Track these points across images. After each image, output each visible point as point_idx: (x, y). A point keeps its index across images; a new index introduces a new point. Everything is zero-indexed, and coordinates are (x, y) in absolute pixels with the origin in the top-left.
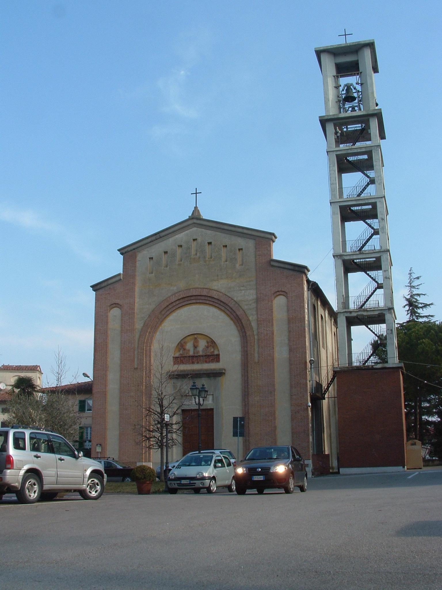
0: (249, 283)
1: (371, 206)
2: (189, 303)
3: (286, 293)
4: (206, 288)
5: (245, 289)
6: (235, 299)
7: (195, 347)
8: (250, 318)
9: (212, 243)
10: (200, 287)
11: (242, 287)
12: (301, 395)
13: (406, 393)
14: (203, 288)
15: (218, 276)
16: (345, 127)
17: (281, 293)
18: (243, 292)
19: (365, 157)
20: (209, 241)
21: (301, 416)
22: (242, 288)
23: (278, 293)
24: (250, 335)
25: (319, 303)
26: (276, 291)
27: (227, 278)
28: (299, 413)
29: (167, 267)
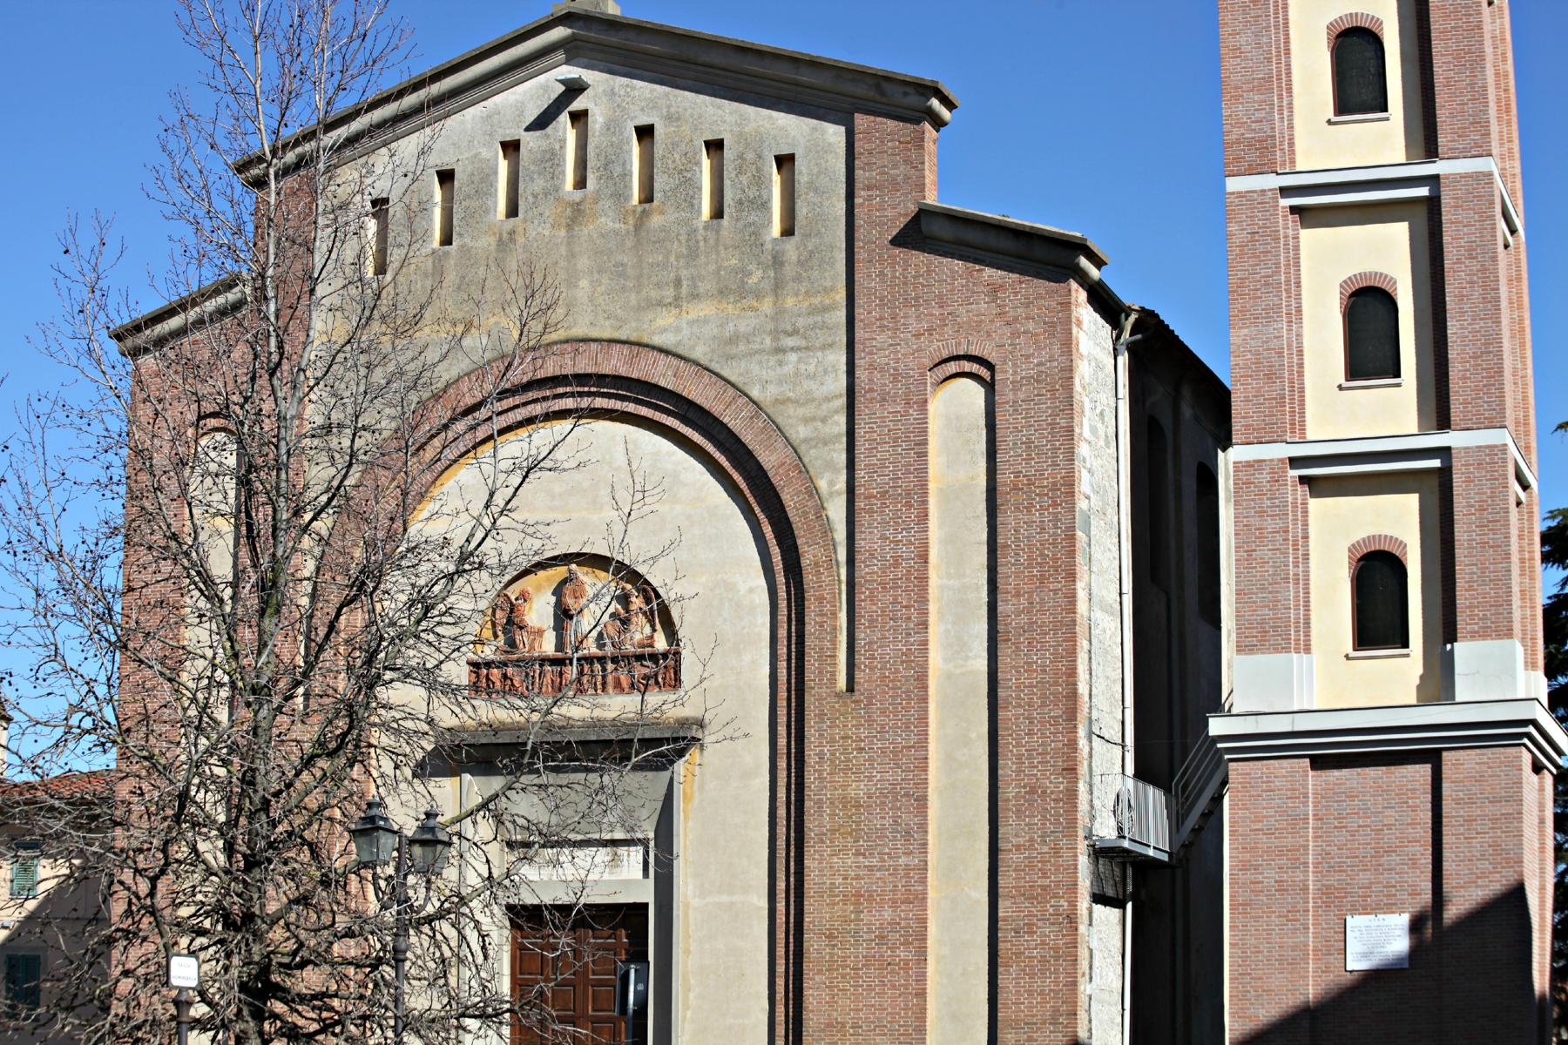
0: (819, 319)
1: (1439, 461)
2: (510, 414)
3: (990, 367)
4: (624, 338)
5: (803, 343)
6: (755, 393)
7: (563, 615)
8: (822, 484)
9: (656, 133)
10: (595, 334)
11: (790, 335)
12: (1046, 849)
13: (1560, 922)
14: (611, 341)
15: (678, 283)
16: (1555, 1031)
17: (967, 366)
18: (793, 357)
19: (1436, 463)
20: (644, 120)
21: (1043, 943)
22: (790, 342)
23: (953, 367)
24: (816, 564)
25: (1187, 412)
26: (945, 354)
27: (721, 292)
28: (1031, 933)
29: (451, 244)
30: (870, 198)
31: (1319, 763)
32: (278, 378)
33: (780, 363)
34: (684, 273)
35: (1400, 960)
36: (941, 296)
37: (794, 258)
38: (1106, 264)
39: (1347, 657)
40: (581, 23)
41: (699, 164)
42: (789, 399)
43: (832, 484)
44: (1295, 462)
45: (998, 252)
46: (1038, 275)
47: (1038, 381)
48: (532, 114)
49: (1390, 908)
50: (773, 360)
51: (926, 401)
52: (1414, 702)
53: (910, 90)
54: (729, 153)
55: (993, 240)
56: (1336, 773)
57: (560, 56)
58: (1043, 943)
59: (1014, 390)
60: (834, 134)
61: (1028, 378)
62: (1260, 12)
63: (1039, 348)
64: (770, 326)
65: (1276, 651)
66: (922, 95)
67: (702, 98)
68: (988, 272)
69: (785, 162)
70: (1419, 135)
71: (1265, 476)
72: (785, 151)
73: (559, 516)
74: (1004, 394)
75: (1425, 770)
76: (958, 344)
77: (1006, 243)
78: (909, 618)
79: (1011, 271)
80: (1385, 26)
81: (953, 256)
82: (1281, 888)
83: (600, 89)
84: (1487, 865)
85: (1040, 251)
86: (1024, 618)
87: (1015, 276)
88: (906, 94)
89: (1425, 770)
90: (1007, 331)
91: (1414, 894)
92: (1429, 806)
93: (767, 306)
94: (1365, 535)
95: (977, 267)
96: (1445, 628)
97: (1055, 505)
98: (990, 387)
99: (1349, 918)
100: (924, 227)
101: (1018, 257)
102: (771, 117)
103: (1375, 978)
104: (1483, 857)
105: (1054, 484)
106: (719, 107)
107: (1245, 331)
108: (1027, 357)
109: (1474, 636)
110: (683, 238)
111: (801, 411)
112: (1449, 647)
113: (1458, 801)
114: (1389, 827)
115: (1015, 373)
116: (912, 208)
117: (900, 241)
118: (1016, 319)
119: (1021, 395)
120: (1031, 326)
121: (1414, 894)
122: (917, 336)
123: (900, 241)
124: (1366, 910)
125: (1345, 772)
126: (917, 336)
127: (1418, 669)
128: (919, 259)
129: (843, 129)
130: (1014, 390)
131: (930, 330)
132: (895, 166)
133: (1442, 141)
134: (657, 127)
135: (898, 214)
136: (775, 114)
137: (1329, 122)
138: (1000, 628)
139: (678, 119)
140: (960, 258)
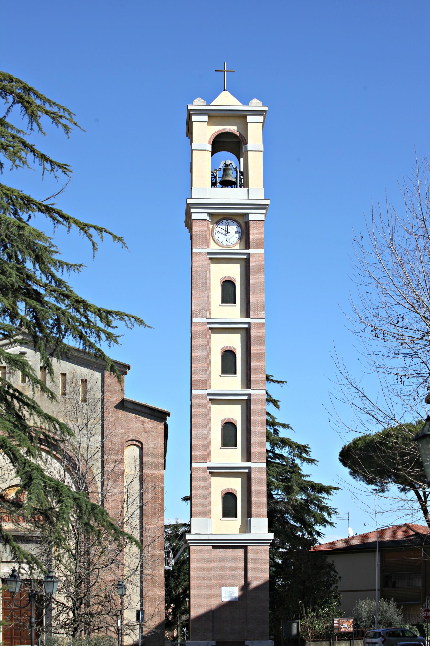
3: (141, 443)
17: (135, 443)
23: (131, 443)
26: (129, 439)
30: (109, 395)
31: (214, 547)
32: (360, 623)
34: (55, 410)
35: (236, 598)
36: (128, 423)
38: (168, 414)
39: (221, 520)
40: (26, 335)
41: (59, 379)
43: (96, 470)
44: (209, 468)
45: (144, 413)
46: (155, 420)
47: (154, 448)
49: (233, 585)
51: (124, 451)
52: (239, 533)
53: (121, 366)
55: (144, 410)
56: (219, 550)
58: (155, 594)
59: (148, 450)
60: (98, 375)
61: (152, 447)
62: (204, 344)
63: (155, 439)
65: (203, 517)
66: (125, 368)
68: (141, 418)
69: (84, 381)
70: (245, 381)
71: (201, 472)
72: (83, 378)
74: (145, 451)
75: (242, 551)
76: (133, 436)
77: (148, 411)
78: (119, 508)
79: (148, 418)
80: (237, 350)
81: (131, 413)
82: (204, 579)
83: (30, 354)
85: (156, 414)
86: (150, 510)
87: (149, 420)
89: (242, 551)
90: (146, 434)
91: (239, 582)
92: (244, 559)
94: (226, 488)
95: (138, 416)
96: (249, 515)
97: (159, 481)
98: (141, 449)
99: (222, 588)
100: (125, 404)
101: (150, 415)
102: (80, 368)
103: (230, 603)
104: (258, 574)
105: (158, 476)
106: (65, 364)
107: (196, 432)
108: (152, 442)
109: (256, 516)
112: (249, 519)
113: (252, 559)
114: (233, 564)
115: (148, 446)
116: (120, 399)
117: (117, 407)
118: (149, 431)
119: (150, 452)
120: (153, 433)
121: (239, 582)
122: (122, 433)
123: (117, 407)
124: (227, 586)
125: (221, 550)
126: (122, 433)
127: (240, 524)
128: (122, 413)
129: (100, 374)
130: (148, 450)
131: (125, 432)
132: (116, 386)
133: (252, 385)
135: (116, 399)
136: (81, 368)
137: (220, 376)
138: (144, 512)
140: (134, 413)
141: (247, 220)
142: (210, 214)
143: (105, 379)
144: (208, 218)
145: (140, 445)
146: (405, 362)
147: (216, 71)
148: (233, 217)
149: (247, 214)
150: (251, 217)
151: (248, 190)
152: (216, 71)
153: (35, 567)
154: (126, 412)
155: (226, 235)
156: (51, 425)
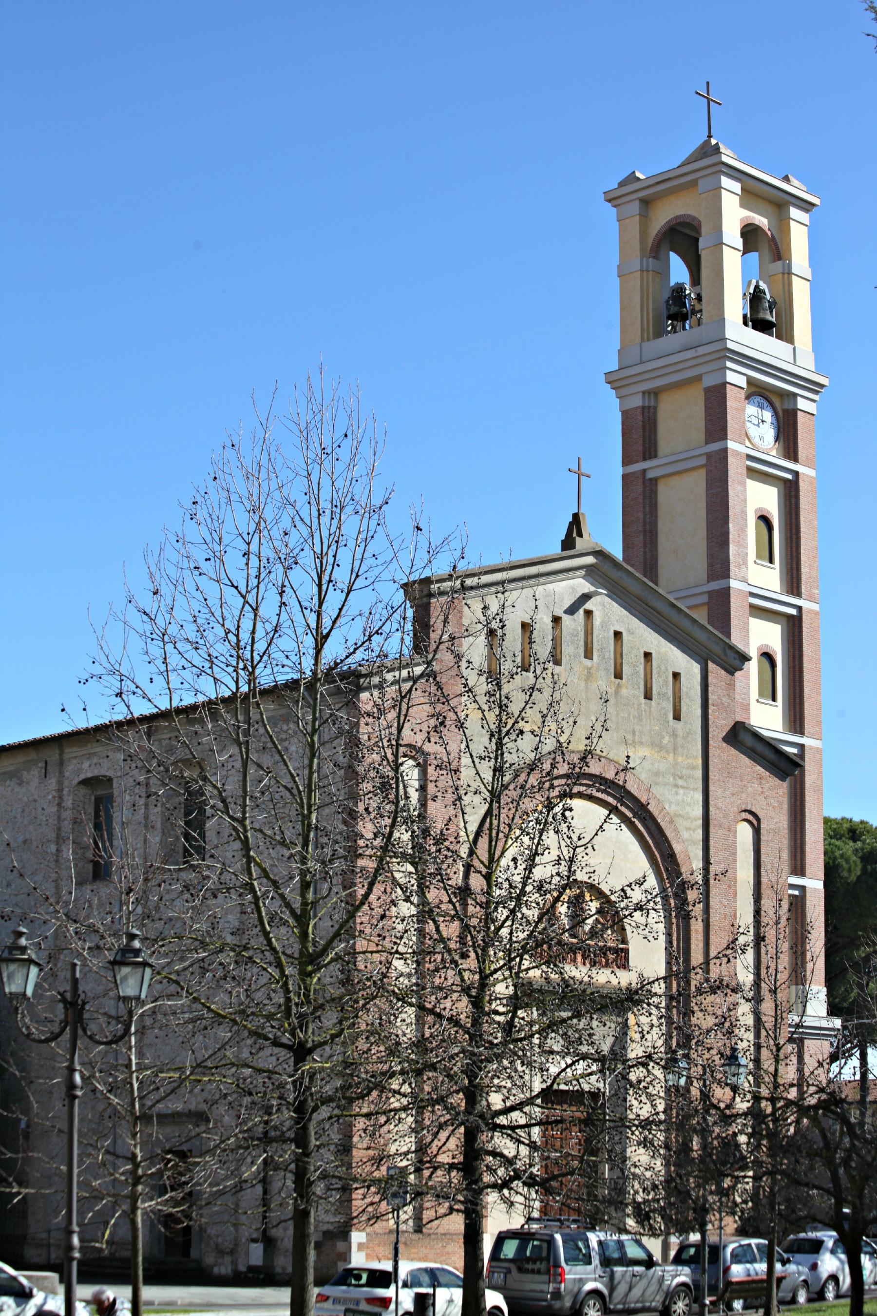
3: (758, 819)
18: (681, 791)
20: (619, 629)
22: (680, 782)
33: (677, 793)
37: (681, 734)
42: (680, 815)
48: (567, 604)
50: (674, 790)
54: (683, 679)
57: (582, 572)
64: (672, 771)
67: (642, 625)
69: (618, 635)
72: (677, 671)
73: (132, 610)
77: (771, 755)
84: (831, 1075)
87: (768, 773)
88: (735, 659)
93: (671, 758)
98: (757, 831)
110: (636, 706)
111: (685, 823)
134: (624, 634)
139: (633, 633)
141: (791, 407)
142: (750, 381)
143: (710, 678)
144: (744, 385)
145: (755, 822)
146: (90, 679)
147: (708, 83)
148: (768, 394)
149: (795, 395)
150: (802, 404)
151: (794, 349)
152: (708, 83)
153: (717, 1020)
154: (737, 752)
155: (758, 425)
156: (506, 740)
